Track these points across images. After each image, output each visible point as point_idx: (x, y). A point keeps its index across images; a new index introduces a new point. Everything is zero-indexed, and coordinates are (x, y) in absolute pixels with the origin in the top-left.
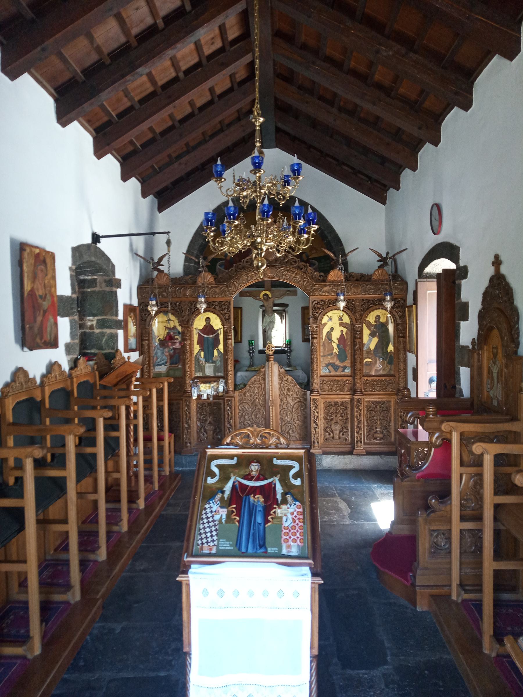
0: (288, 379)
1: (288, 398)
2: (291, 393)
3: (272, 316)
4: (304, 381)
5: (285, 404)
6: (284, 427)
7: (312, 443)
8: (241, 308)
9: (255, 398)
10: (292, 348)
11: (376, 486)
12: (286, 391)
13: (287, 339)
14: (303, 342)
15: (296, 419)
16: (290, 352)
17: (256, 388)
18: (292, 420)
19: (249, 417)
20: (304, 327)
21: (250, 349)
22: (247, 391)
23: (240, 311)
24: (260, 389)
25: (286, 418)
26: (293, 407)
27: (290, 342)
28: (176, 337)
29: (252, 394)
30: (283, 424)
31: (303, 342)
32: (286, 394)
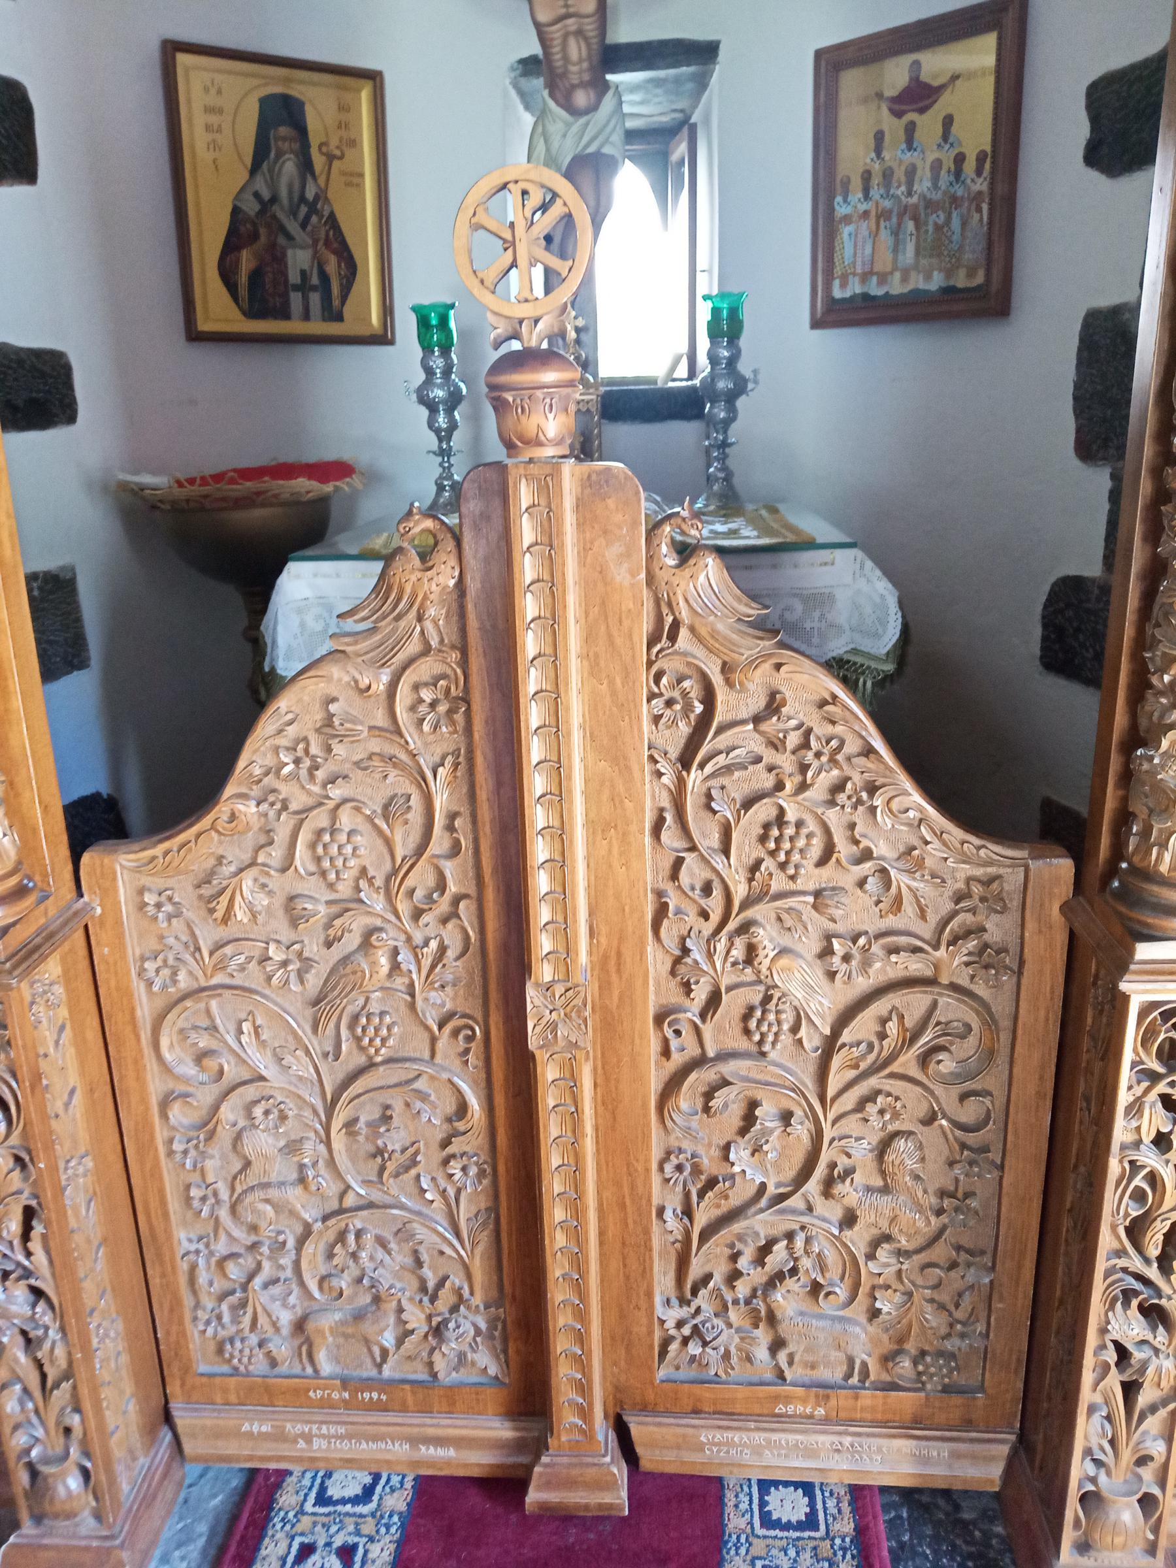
0: (773, 705)
1: (766, 937)
2: (811, 877)
3: (594, 108)
4: (867, 645)
5: (732, 1005)
6: (717, 1246)
7: (1073, 1507)
8: (374, 77)
9: (352, 941)
10: (744, 368)
11: (1082, 1080)
12: (744, 846)
13: (704, 285)
14: (816, 324)
15: (866, 1175)
16: (731, 398)
17: (346, 819)
18: (813, 1186)
19: (293, 1147)
20: (831, 209)
21: (429, 372)
22: (237, 854)
23: (365, 95)
24: (404, 841)
25: (740, 1155)
26: (830, 1046)
27: (734, 313)
28: (596, 526)
29: (312, 886)
30: (702, 1219)
31: (816, 324)
32: (740, 891)
